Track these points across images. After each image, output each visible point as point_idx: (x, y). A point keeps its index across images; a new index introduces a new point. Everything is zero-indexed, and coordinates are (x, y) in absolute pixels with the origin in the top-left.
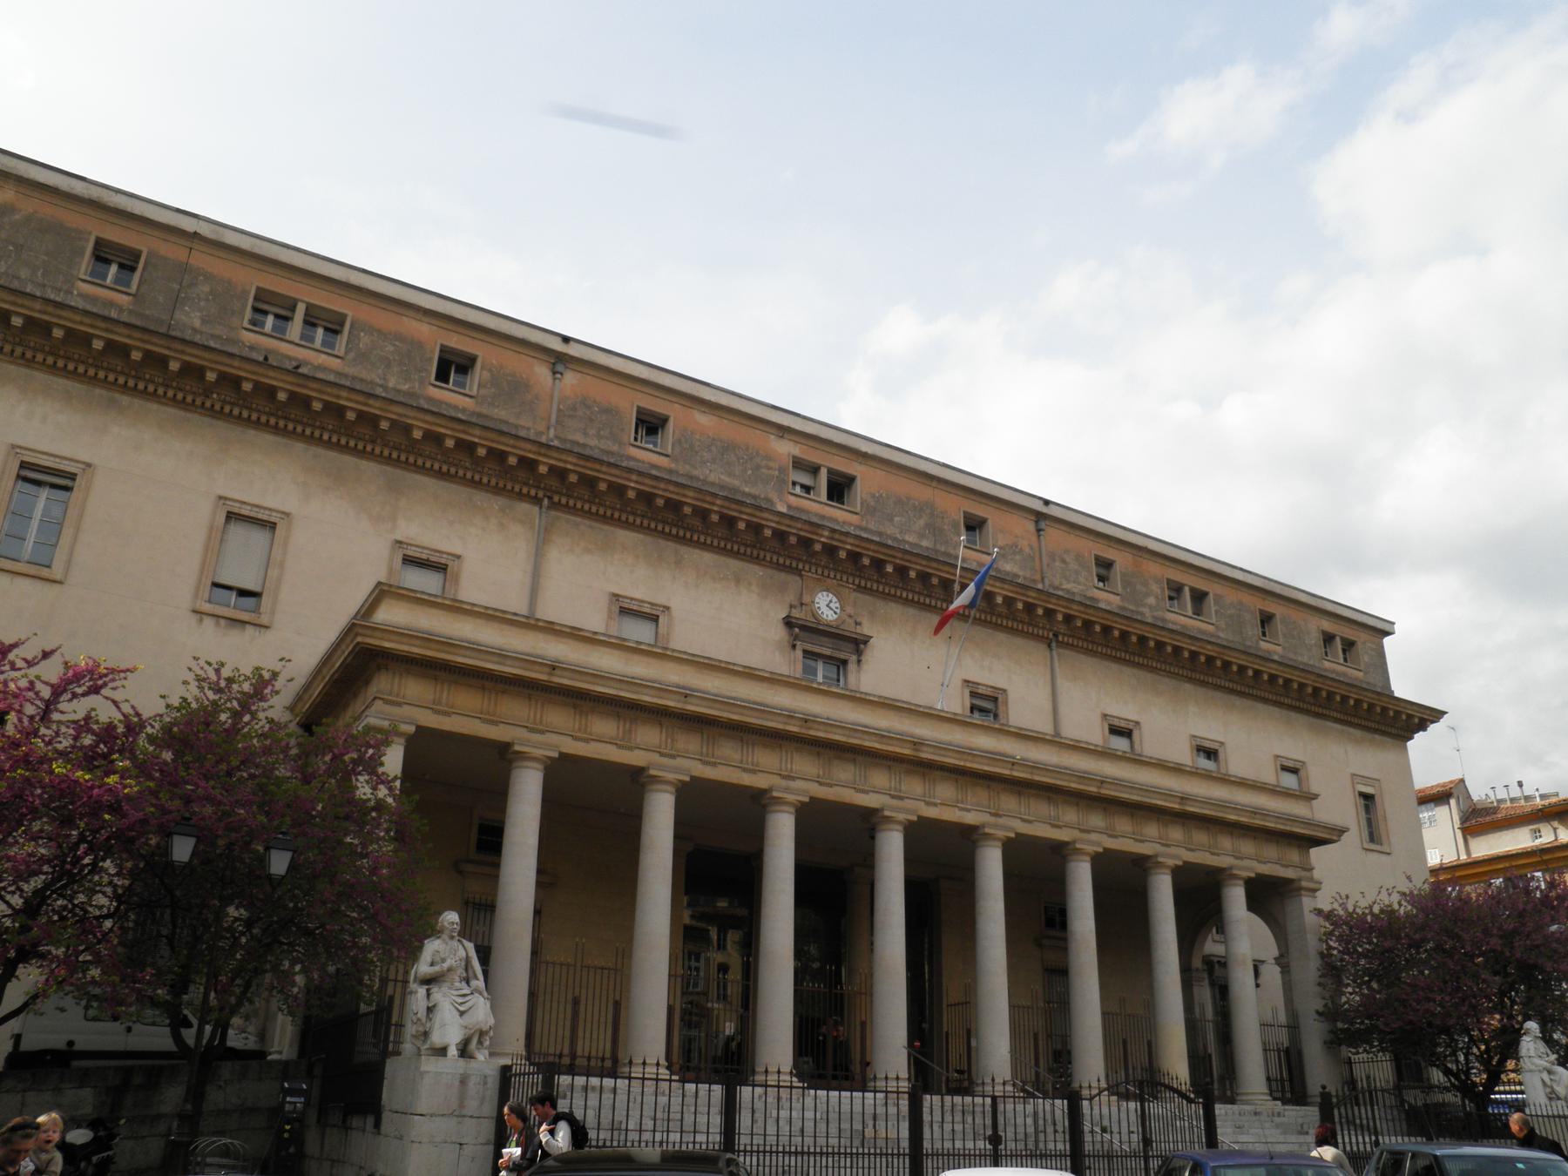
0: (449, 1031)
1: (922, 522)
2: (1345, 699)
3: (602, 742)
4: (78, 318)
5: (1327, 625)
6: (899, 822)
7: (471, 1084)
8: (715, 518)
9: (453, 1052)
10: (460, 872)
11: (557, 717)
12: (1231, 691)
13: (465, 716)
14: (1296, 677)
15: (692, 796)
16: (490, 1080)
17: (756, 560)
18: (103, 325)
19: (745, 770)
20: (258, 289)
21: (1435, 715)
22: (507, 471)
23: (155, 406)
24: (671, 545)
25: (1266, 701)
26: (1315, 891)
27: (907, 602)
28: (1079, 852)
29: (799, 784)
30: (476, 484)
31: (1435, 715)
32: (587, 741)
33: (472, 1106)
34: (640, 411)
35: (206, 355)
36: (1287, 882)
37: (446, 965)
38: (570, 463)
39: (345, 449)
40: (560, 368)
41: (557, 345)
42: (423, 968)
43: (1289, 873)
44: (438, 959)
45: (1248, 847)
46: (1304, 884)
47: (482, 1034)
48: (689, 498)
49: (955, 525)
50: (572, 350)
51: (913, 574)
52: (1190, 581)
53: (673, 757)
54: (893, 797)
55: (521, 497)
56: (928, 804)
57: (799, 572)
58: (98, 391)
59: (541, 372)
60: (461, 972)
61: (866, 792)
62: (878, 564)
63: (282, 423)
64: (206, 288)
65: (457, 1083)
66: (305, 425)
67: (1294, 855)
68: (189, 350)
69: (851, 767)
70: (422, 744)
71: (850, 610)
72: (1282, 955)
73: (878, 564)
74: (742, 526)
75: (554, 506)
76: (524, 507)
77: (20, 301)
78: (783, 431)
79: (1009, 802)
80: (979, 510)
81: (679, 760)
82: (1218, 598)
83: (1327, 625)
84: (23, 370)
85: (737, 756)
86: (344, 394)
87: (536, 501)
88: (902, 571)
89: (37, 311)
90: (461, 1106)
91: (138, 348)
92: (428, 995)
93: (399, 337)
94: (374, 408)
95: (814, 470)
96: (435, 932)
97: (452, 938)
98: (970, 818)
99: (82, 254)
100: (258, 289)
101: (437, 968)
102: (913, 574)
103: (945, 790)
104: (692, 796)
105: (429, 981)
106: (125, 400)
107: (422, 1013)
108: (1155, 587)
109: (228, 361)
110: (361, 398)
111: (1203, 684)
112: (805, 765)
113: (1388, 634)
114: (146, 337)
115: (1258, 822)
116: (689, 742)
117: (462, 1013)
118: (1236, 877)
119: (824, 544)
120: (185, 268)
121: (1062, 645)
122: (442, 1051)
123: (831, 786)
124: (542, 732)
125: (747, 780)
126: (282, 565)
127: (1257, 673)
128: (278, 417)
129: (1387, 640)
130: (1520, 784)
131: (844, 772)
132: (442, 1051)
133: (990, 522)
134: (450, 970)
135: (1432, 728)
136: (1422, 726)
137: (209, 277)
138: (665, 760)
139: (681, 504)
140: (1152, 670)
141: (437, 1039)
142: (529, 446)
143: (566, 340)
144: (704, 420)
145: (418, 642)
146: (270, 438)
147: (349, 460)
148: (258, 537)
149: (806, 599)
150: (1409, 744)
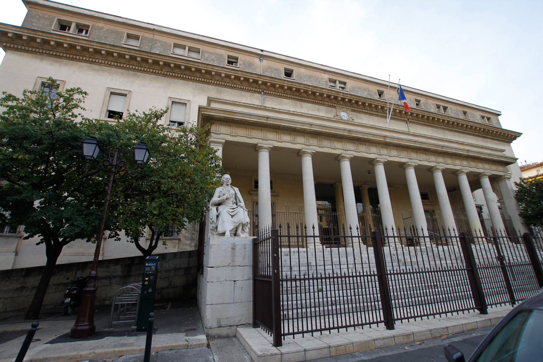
0: (226, 224)
1: (366, 93)
2: (493, 131)
3: (286, 142)
4: (120, 49)
5: (482, 114)
6: (382, 162)
7: (237, 248)
8: (310, 92)
9: (228, 233)
10: (251, 194)
11: (271, 135)
12: (459, 132)
13: (241, 136)
14: (478, 126)
15: (317, 157)
16: (247, 247)
17: (323, 105)
18: (127, 51)
19: (332, 149)
20: (174, 43)
21: (519, 134)
22: (250, 84)
23: (148, 75)
24: (299, 102)
25: (469, 134)
26: (510, 178)
27: (366, 113)
28: (437, 169)
29: (349, 152)
30: (242, 89)
31: (519, 134)
32: (281, 142)
33: (239, 260)
34: (285, 69)
35: (159, 57)
36: (500, 176)
37: (225, 197)
38: (267, 80)
39: (204, 82)
40: (261, 59)
41: (260, 52)
42: (215, 199)
43: (501, 174)
44: (221, 195)
45: (487, 166)
46: (506, 176)
47: (243, 225)
48: (302, 87)
49: (375, 93)
50: (264, 53)
51: (367, 104)
52: (442, 104)
53: (309, 146)
54: (379, 155)
55: (255, 92)
56: (390, 156)
57: (335, 107)
58: (131, 72)
59: (256, 60)
60: (233, 199)
61: (370, 154)
62: (357, 102)
63: (184, 76)
64: (160, 44)
65: (230, 250)
66: (191, 76)
67: (501, 168)
68: (153, 56)
69: (364, 147)
70: (227, 145)
71: (350, 116)
72: (500, 199)
73: (357, 102)
74: (318, 94)
75: (265, 94)
76: (257, 95)
77: (103, 46)
78: (325, 71)
79: (414, 155)
80: (381, 89)
81: (311, 147)
82: (451, 109)
83: (482, 114)
84: (109, 68)
85: (329, 145)
86: (200, 65)
87: (260, 93)
88: (364, 104)
89: (108, 48)
90: (233, 261)
91: (139, 57)
92: (217, 210)
93: (217, 54)
94: (210, 68)
95: (335, 82)
96: (220, 184)
97: (228, 185)
98: (403, 160)
99: (123, 37)
100: (174, 43)
101: (221, 198)
102: (367, 104)
103: (394, 152)
104: (317, 157)
105: (219, 204)
106: (139, 74)
107: (214, 219)
108: (433, 106)
109: (165, 58)
110: (205, 66)
111: (451, 130)
112: (350, 146)
113: (499, 115)
114: (140, 53)
115: (491, 157)
116: (313, 141)
117: (232, 216)
118: (485, 175)
119: (341, 98)
120: (153, 40)
121: (410, 122)
122: (223, 234)
123: (359, 152)
124: (267, 140)
125: (333, 151)
126: (189, 114)
127: (467, 126)
128: (183, 75)
129: (499, 117)
130: (525, 161)
131: (362, 148)
132: (223, 234)
133: (385, 92)
134: (227, 199)
135: (518, 139)
136: (515, 139)
137: (160, 41)
138: (307, 147)
139: (300, 89)
140: (436, 127)
141: (220, 230)
142: (255, 76)
143: (262, 51)
144: (303, 70)
145: (222, 112)
146: (182, 81)
147: (206, 86)
148: (182, 108)
149: (338, 114)
150: (511, 144)
